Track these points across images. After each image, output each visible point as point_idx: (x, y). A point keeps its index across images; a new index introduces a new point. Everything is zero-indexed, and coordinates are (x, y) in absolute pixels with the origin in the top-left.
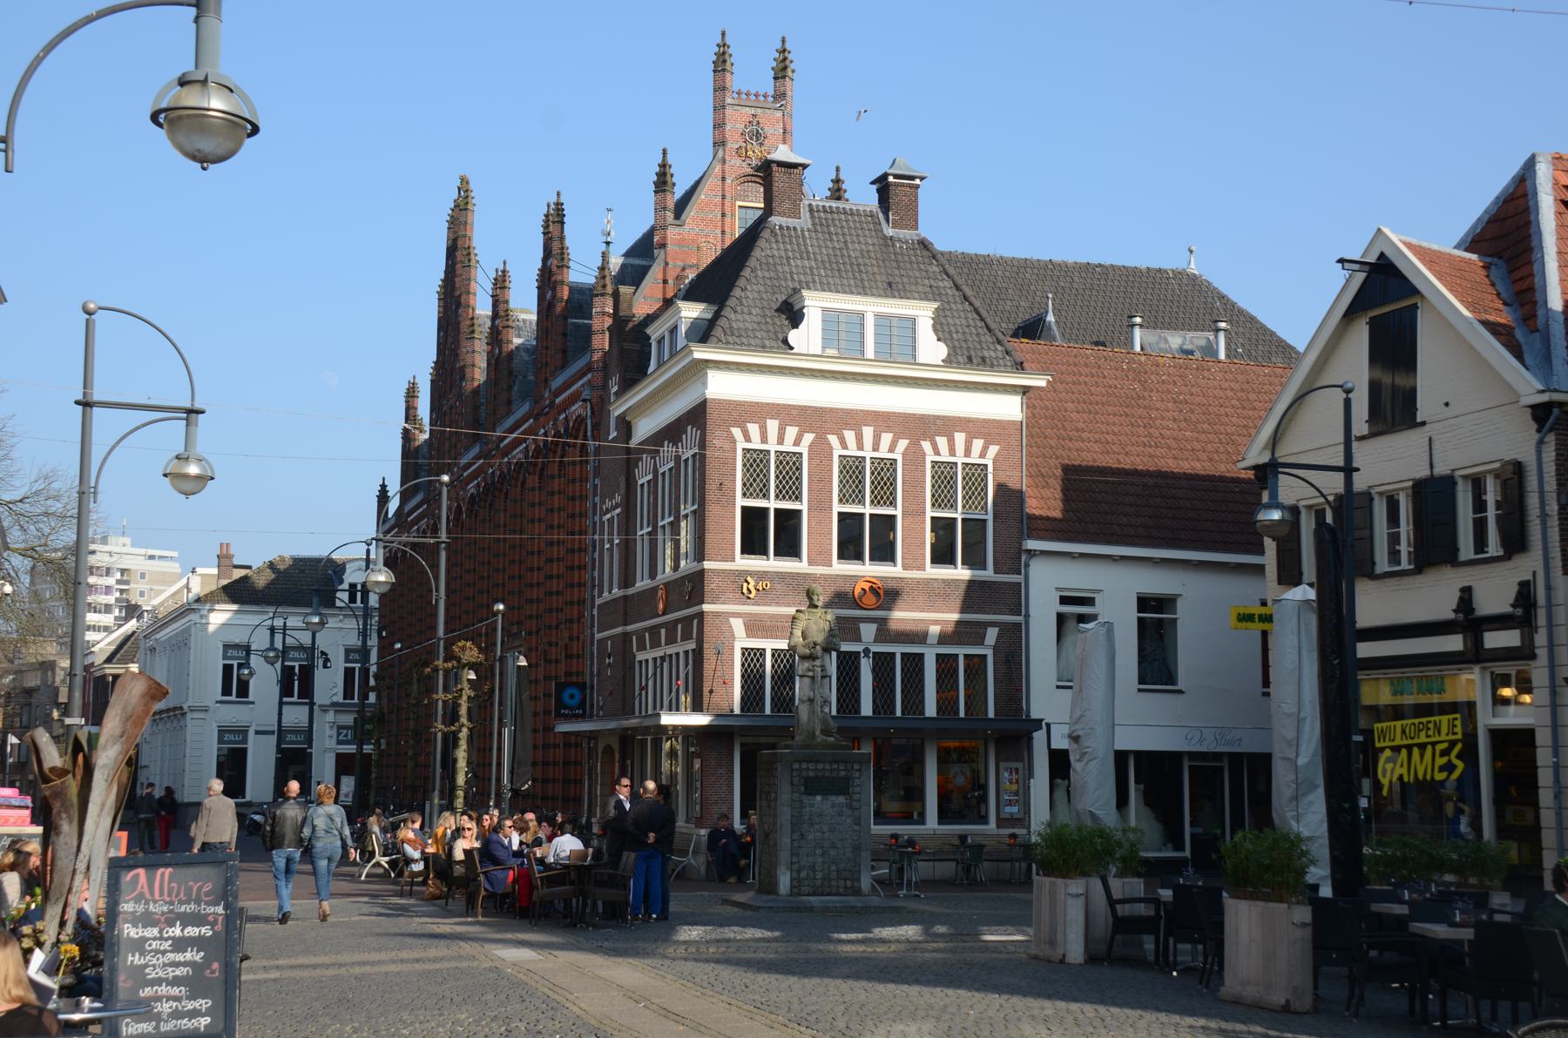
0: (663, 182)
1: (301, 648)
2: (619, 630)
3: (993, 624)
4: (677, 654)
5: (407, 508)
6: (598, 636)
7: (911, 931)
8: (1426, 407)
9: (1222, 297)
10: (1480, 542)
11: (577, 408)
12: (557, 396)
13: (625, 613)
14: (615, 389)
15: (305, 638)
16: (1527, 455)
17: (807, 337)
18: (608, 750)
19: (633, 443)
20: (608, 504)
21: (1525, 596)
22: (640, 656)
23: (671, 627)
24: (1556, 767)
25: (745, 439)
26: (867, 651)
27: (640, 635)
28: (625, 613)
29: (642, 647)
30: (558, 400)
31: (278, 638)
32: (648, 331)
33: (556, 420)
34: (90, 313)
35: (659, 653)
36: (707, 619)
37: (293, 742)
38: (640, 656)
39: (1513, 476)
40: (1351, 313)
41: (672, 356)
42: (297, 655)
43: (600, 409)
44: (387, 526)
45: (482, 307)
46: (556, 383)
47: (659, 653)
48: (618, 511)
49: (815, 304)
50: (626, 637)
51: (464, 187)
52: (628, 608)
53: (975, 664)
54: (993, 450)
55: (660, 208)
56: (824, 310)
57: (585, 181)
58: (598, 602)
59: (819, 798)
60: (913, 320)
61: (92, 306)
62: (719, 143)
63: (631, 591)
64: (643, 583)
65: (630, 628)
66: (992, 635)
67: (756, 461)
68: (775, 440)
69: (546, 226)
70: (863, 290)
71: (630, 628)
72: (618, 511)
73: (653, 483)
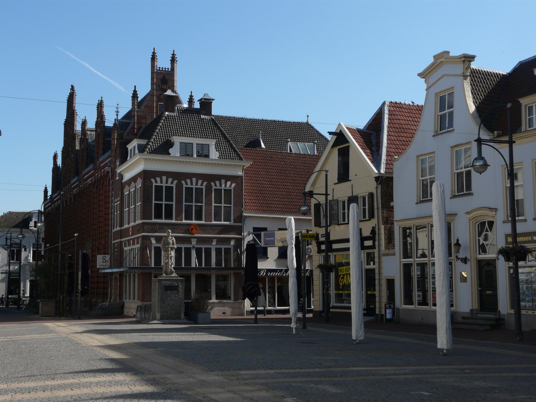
1: (16, 244)
2: (119, 240)
5: (54, 196)
6: (113, 242)
12: (101, 163)
13: (121, 235)
14: (118, 164)
15: (17, 241)
16: (374, 191)
17: (175, 151)
19: (124, 181)
20: (116, 200)
21: (373, 231)
23: (133, 240)
24: (379, 279)
27: (125, 242)
28: (121, 235)
29: (125, 246)
30: (101, 165)
31: (9, 242)
32: (128, 146)
33: (101, 171)
35: (130, 248)
37: (163, 63)
38: (125, 249)
39: (371, 195)
42: (15, 246)
43: (114, 171)
44: (46, 202)
45: (78, 127)
46: (101, 159)
47: (130, 248)
49: (177, 140)
50: (121, 242)
51: (73, 88)
53: (227, 251)
54: (234, 185)
55: (133, 104)
57: (114, 92)
58: (113, 231)
59: (169, 292)
63: (122, 228)
64: (126, 226)
66: (232, 243)
70: (193, 136)
71: (122, 240)
73: (129, 194)
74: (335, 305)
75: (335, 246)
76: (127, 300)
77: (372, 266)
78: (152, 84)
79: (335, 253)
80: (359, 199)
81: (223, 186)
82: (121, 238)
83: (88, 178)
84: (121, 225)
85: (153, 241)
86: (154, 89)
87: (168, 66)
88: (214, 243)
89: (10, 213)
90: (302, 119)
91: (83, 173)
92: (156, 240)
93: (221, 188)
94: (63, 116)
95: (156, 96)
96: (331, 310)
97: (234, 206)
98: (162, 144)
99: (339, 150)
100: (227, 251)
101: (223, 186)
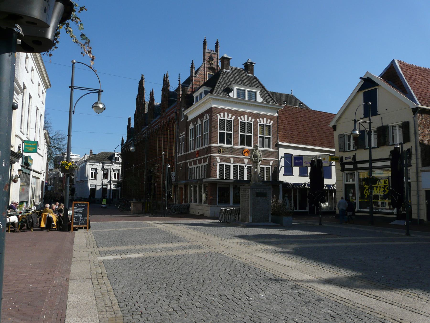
0: (192, 67)
2: (185, 161)
3: (272, 160)
4: (202, 166)
6: (178, 163)
8: (379, 111)
9: (298, 100)
10: (349, 149)
11: (172, 115)
17: (233, 94)
18: (181, 188)
19: (188, 120)
22: (190, 167)
25: (220, 116)
32: (193, 95)
34: (74, 63)
35: (196, 166)
36: (212, 157)
38: (190, 167)
40: (360, 90)
41: (200, 99)
43: (179, 116)
45: (147, 100)
47: (196, 166)
49: (235, 89)
50: (186, 163)
52: (186, 157)
54: (272, 122)
56: (237, 89)
57: (177, 67)
58: (178, 156)
59: (259, 198)
60: (255, 92)
61: (75, 61)
62: (204, 60)
63: (187, 153)
65: (187, 161)
66: (271, 163)
67: (222, 121)
68: (227, 117)
69: (164, 79)
71: (187, 161)
74: (360, 210)
75: (359, 166)
76: (193, 203)
77: (351, 181)
79: (359, 171)
80: (390, 128)
83: (155, 125)
84: (186, 150)
89: (102, 153)
90: (288, 92)
91: (142, 130)
96: (356, 214)
99: (364, 93)
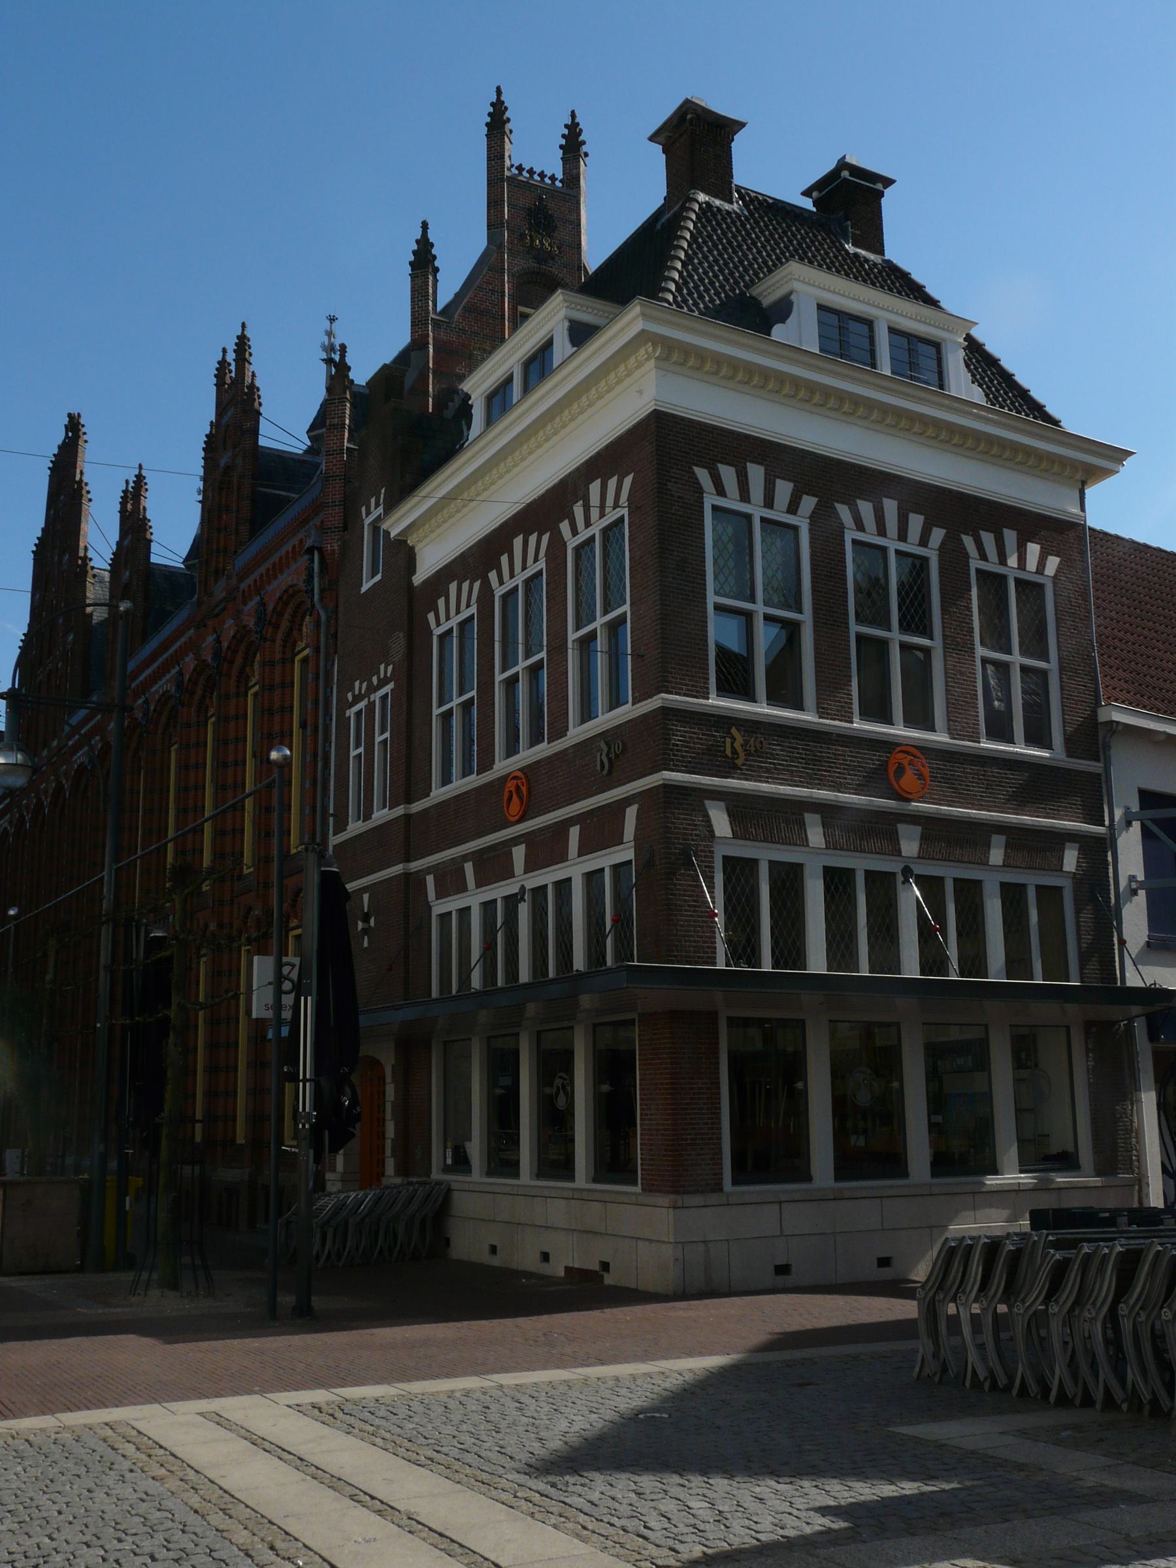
2: (397, 869)
7: (128, 1199)
12: (241, 579)
22: (439, 907)
26: (907, 872)
32: (466, 387)
37: (535, 151)
45: (100, 537)
48: (391, 686)
51: (74, 425)
58: (334, 840)
63: (417, 807)
65: (415, 866)
71: (415, 866)
72: (391, 686)
78: (494, 224)
81: (1013, 561)
82: (408, 860)
85: (721, 823)
86: (501, 246)
87: (552, 165)
88: (996, 856)
92: (735, 817)
93: (1000, 570)
94: (32, 521)
95: (511, 275)
97: (1062, 669)
98: (722, 304)
100: (1050, 896)
101: (1013, 561)
